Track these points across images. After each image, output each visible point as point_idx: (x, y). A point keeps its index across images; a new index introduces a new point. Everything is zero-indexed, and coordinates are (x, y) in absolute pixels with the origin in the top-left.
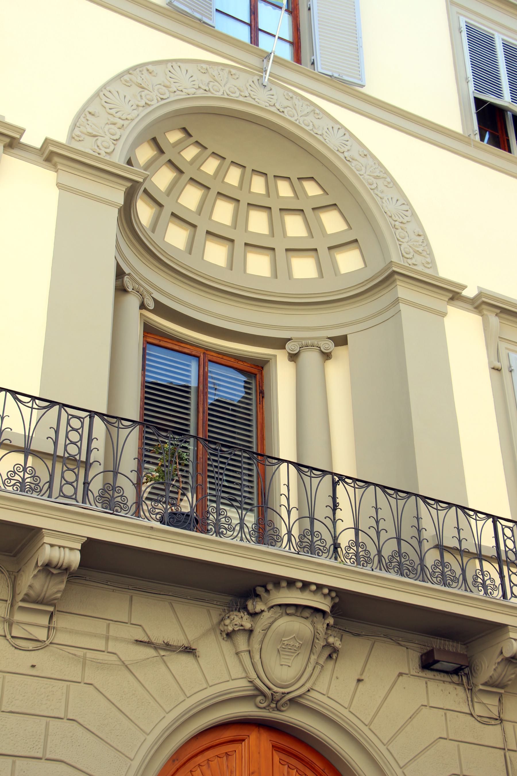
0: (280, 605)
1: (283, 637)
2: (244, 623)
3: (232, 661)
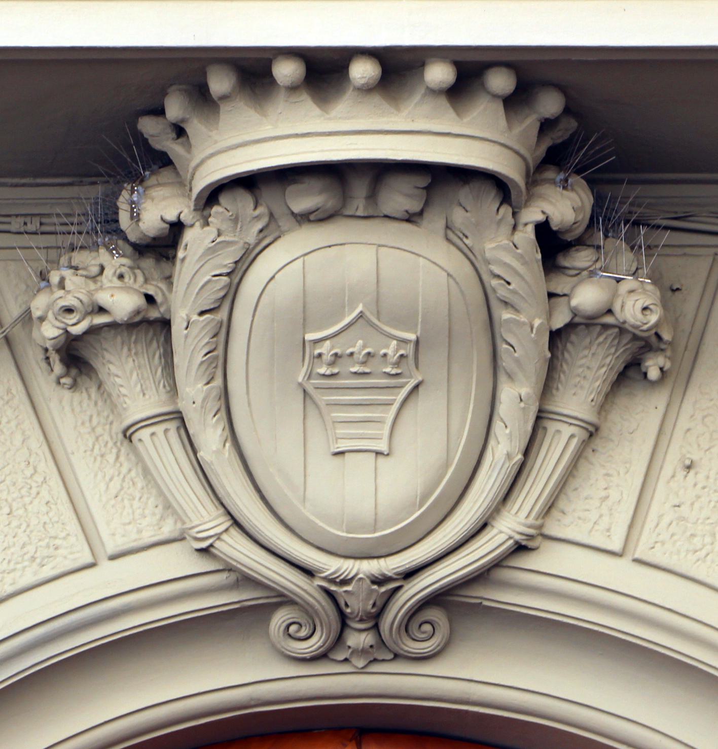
0: (249, 183)
1: (305, 326)
2: (104, 298)
3: (100, 476)
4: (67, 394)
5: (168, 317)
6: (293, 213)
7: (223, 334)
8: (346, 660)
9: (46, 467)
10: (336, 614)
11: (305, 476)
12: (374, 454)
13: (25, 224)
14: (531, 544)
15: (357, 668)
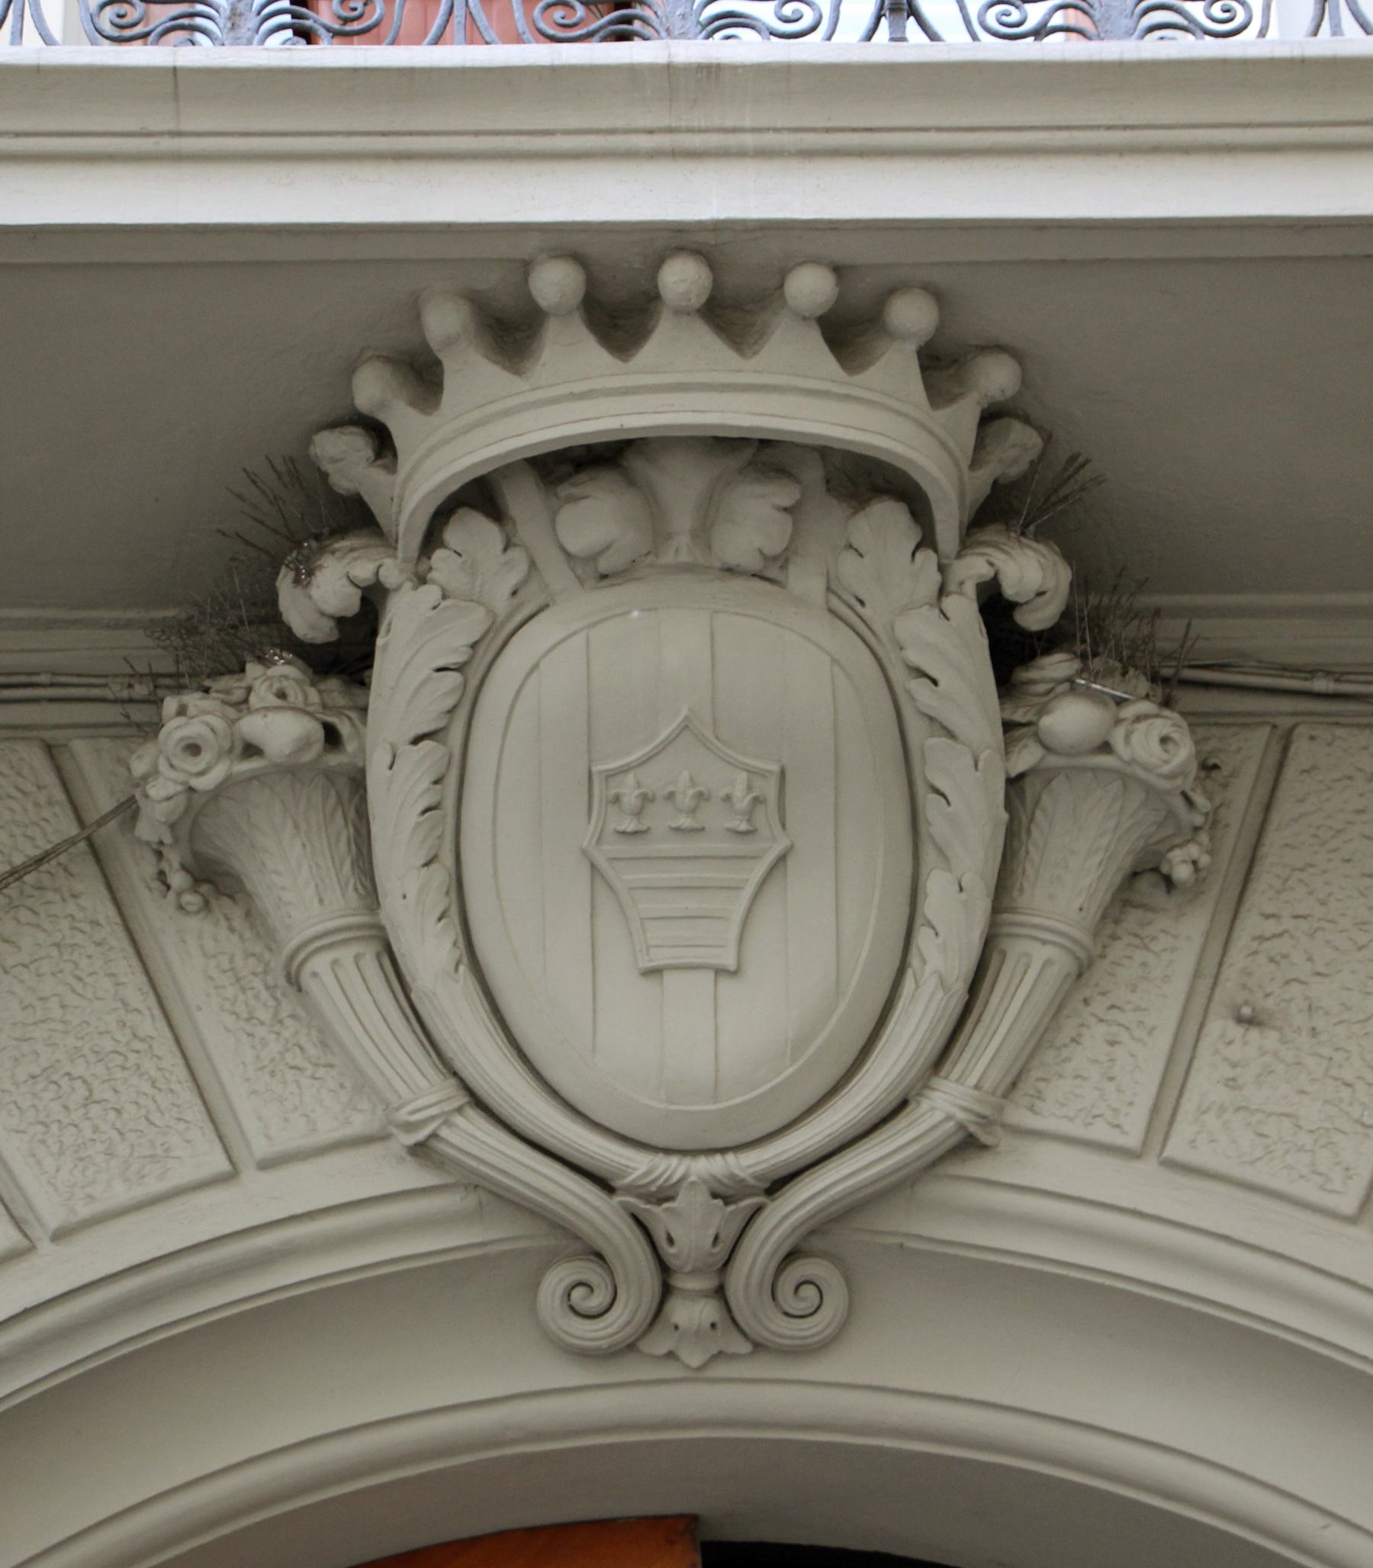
2: (253, 726)
4: (194, 923)
5: (360, 764)
6: (568, 555)
7: (455, 778)
8: (671, 1355)
9: (151, 1025)
10: (652, 1261)
11: (595, 1011)
12: (711, 975)
13: (130, 686)
14: (984, 1138)
15: (687, 1367)
